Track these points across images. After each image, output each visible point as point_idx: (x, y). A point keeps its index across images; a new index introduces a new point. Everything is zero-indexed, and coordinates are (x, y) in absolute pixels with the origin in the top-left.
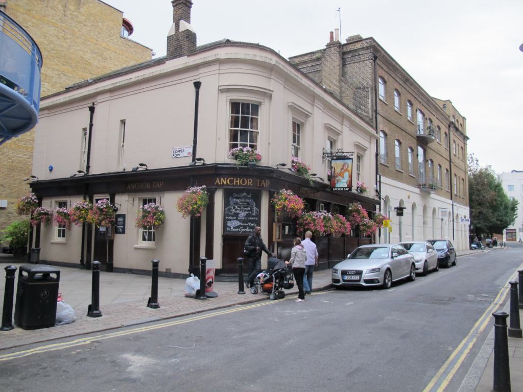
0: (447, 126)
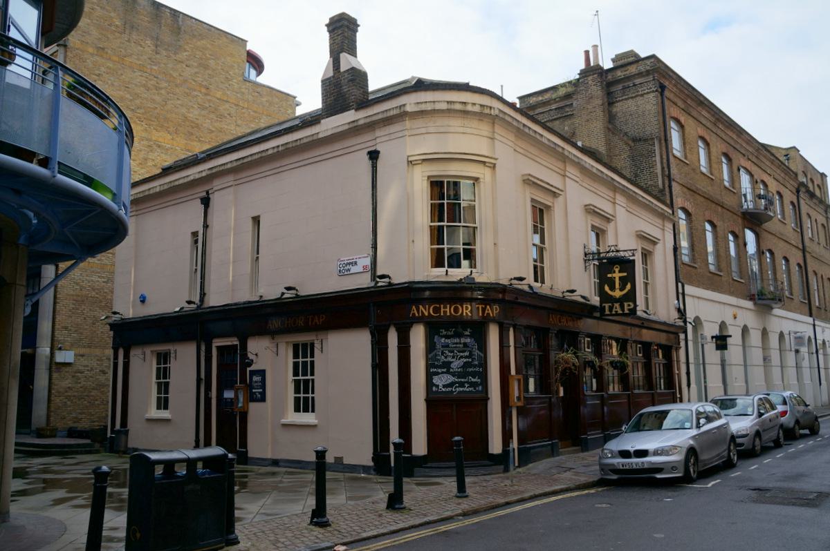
0: (794, 191)
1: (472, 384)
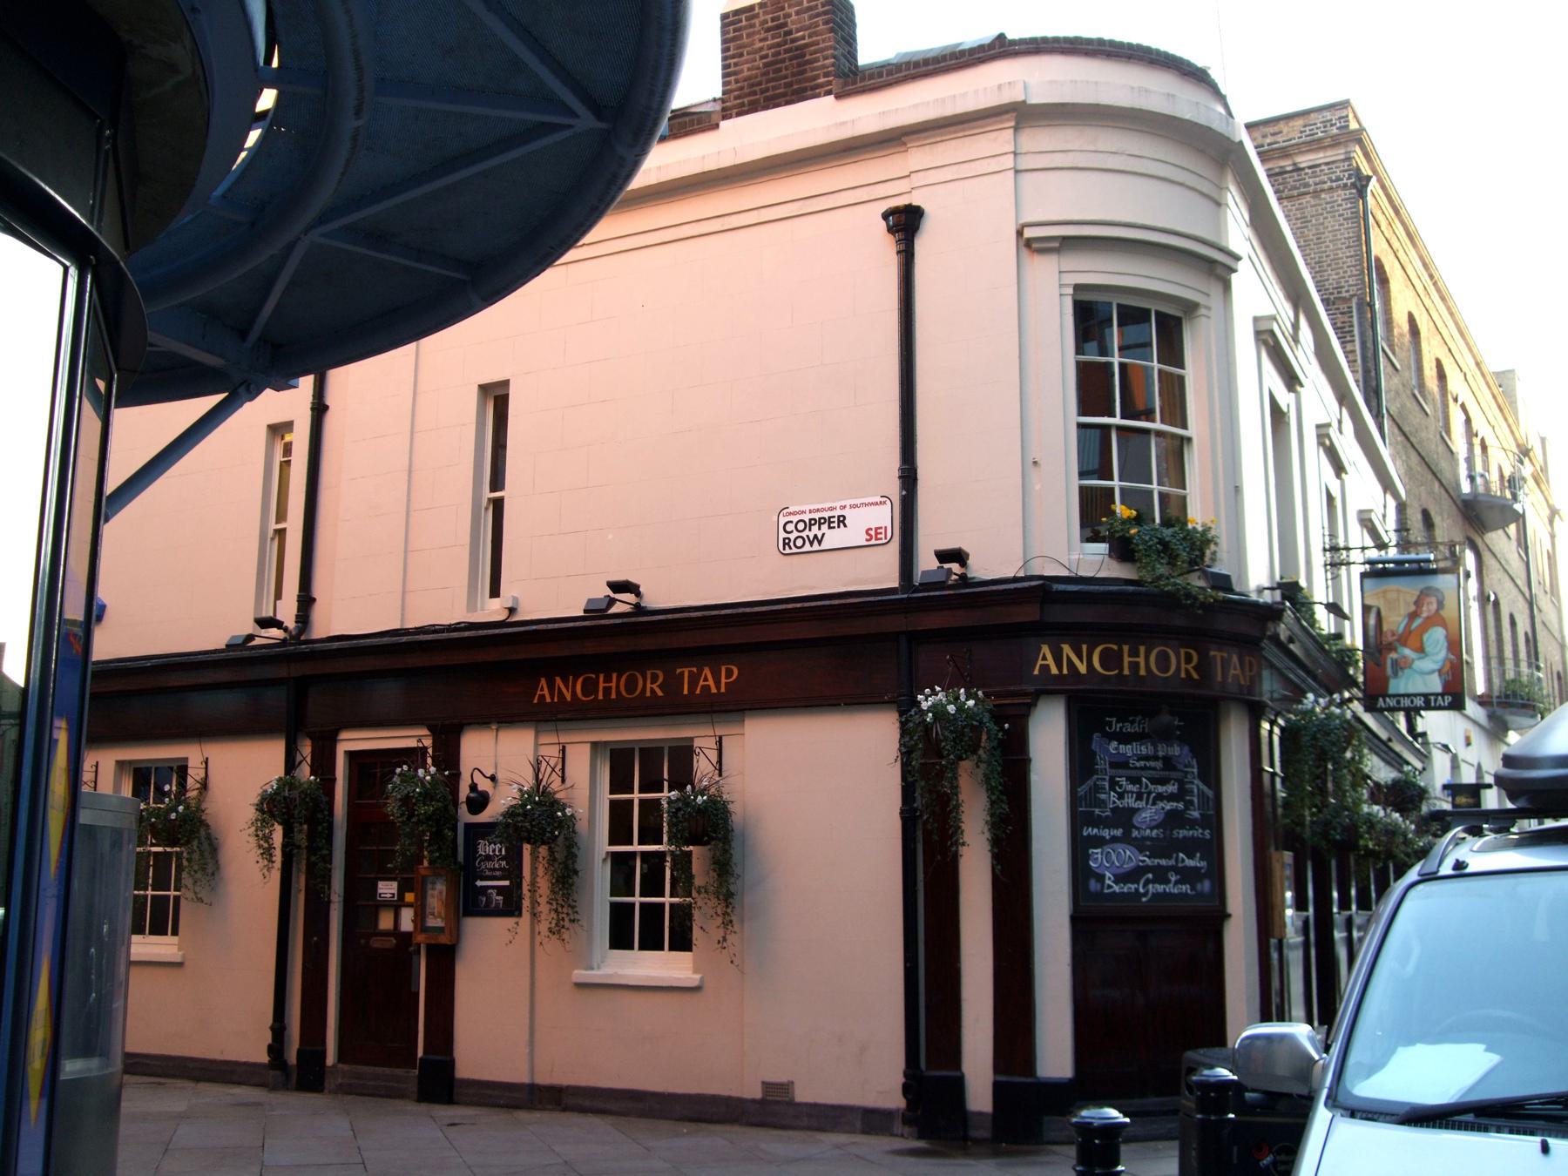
1: (1188, 875)
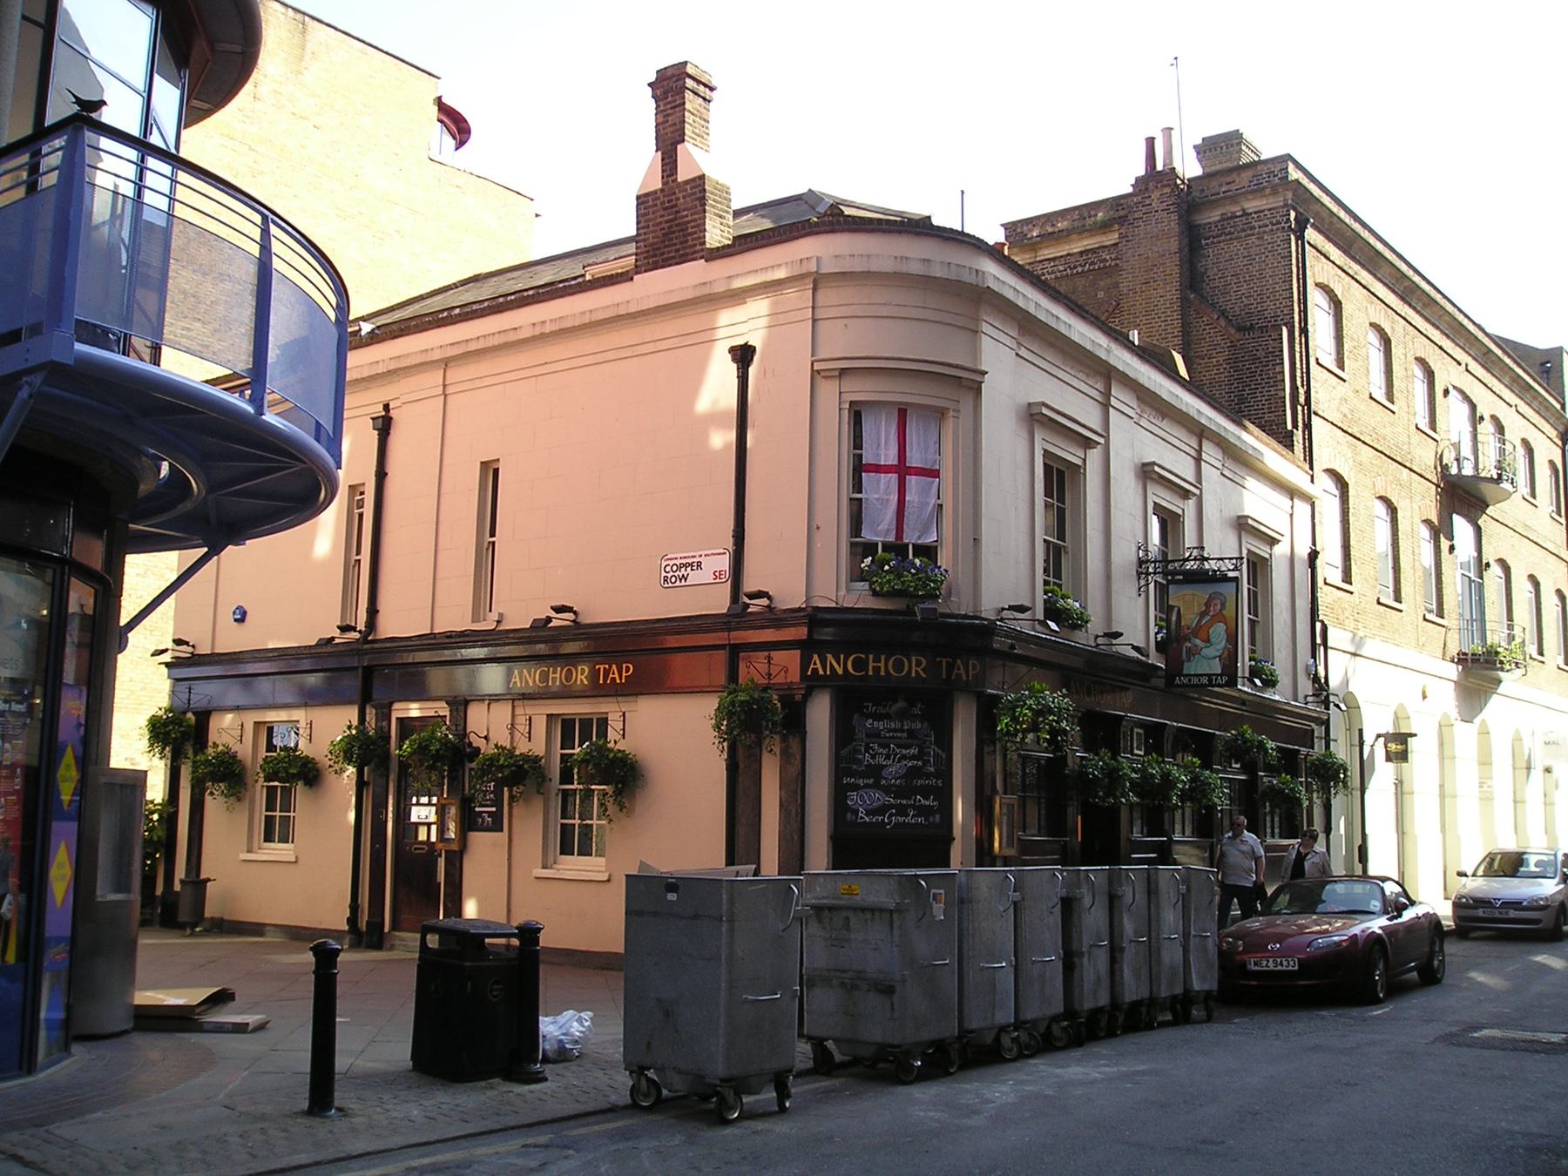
1: (922, 811)
